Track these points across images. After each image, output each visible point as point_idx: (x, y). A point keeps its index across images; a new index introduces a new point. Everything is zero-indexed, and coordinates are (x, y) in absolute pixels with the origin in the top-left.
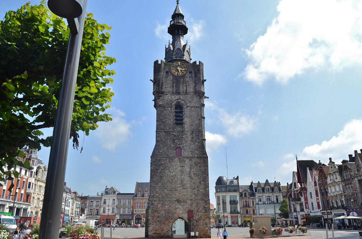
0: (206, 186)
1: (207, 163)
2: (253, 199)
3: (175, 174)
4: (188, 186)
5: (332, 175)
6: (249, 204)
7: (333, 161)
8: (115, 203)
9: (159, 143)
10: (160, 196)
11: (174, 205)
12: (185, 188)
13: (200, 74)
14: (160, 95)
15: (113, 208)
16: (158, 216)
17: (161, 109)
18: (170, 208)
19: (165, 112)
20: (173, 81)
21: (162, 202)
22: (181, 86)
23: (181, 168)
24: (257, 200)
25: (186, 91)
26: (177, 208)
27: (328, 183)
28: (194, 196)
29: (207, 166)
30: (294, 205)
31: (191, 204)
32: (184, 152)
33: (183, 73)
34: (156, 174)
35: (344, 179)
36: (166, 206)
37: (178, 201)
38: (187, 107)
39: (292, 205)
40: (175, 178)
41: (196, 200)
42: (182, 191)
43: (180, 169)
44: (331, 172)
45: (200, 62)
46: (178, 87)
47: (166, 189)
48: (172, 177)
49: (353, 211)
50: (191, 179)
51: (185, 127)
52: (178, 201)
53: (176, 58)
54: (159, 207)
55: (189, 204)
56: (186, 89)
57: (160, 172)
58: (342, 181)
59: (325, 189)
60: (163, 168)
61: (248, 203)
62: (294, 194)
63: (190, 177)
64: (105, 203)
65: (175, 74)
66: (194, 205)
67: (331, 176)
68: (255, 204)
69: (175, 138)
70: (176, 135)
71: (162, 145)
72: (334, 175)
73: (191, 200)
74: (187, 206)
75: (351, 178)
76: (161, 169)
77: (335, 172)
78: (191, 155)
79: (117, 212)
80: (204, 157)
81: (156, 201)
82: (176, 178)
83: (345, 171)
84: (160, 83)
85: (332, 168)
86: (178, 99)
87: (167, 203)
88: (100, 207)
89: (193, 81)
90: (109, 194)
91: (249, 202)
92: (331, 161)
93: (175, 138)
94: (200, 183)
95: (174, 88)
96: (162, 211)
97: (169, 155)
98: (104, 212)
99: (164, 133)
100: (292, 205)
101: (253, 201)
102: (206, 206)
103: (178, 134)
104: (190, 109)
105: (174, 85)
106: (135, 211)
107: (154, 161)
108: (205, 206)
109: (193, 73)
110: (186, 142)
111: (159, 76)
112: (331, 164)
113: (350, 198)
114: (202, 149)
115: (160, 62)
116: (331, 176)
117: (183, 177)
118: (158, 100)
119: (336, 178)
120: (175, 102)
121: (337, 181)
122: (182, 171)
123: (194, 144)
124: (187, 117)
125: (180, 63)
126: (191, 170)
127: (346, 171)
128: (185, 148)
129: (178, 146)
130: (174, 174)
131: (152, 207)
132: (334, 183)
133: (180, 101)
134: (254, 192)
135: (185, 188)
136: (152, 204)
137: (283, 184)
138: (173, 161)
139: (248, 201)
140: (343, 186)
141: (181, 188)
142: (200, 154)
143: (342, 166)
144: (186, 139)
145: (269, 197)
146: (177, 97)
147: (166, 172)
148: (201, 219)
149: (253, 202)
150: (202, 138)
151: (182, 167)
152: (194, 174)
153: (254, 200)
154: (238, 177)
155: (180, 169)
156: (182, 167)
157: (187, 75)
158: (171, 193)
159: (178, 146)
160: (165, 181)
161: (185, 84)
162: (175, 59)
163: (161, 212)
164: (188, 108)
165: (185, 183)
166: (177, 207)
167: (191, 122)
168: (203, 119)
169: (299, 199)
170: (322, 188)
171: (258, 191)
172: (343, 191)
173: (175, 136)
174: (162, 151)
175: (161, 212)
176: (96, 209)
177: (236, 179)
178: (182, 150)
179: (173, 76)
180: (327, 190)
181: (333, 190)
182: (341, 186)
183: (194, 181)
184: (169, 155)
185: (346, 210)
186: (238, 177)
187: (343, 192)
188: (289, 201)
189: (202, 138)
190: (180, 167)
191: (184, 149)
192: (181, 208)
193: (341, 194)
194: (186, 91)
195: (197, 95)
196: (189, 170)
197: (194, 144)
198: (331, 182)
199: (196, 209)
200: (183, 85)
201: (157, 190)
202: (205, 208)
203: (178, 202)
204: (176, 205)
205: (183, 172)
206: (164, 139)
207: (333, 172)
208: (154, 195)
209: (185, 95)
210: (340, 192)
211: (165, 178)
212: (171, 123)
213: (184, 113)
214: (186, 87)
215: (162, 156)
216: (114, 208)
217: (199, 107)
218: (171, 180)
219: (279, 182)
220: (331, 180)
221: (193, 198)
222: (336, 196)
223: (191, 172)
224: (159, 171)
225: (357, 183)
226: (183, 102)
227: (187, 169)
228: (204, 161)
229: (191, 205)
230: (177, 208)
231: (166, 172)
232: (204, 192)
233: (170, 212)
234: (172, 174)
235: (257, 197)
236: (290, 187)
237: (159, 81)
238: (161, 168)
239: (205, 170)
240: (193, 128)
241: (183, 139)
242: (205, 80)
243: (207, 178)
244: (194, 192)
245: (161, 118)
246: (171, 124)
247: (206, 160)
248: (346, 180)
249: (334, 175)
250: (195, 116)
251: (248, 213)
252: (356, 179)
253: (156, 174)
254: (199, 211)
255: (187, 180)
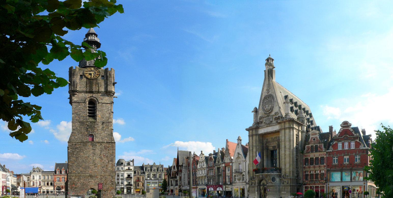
0: (113, 165)
1: (114, 147)
2: (143, 176)
3: (88, 155)
4: (99, 164)
5: (201, 163)
6: (140, 179)
7: (203, 153)
8: (40, 179)
9: (74, 131)
10: (76, 173)
11: (88, 179)
12: (96, 167)
13: (112, 78)
14: (75, 93)
15: (39, 182)
16: (75, 187)
17: (75, 104)
18: (84, 181)
19: (80, 107)
20: (87, 83)
21: (78, 177)
22: (94, 86)
23: (93, 151)
24: (146, 176)
25: (98, 90)
26: (90, 182)
27: (198, 168)
28: (103, 173)
29: (115, 149)
30: (171, 181)
31: (101, 179)
32: (95, 139)
33: (96, 76)
34: (73, 155)
35: (209, 166)
36: (81, 180)
37: (91, 176)
38: (99, 103)
39: (170, 181)
40: (88, 159)
41: (105, 175)
42: (94, 168)
43: (92, 151)
44: (201, 161)
45: (111, 69)
46: (91, 87)
47: (81, 167)
48: (86, 158)
49: (211, 187)
50: (101, 160)
51: (97, 119)
52: (91, 176)
53: (89, 65)
54: (76, 180)
55: (100, 178)
56: (99, 89)
57: (76, 154)
58: (207, 167)
59: (195, 172)
60: (78, 151)
61: (140, 179)
62: (173, 174)
63: (101, 158)
64: (34, 179)
65: (88, 77)
66: (103, 179)
67: (201, 163)
68: (144, 180)
69: (88, 127)
70: (89, 125)
71: (77, 133)
72: (203, 163)
73: (101, 175)
74: (98, 180)
75: (213, 165)
76: (77, 152)
77: (203, 161)
78: (101, 141)
79: (43, 185)
80: (112, 143)
81: (73, 176)
82: (89, 159)
83: (210, 161)
84: (75, 84)
85: (202, 158)
86: (91, 97)
87: (82, 178)
88: (31, 181)
89: (105, 83)
90: (36, 172)
91: (140, 178)
92: (202, 153)
93: (88, 127)
94: (109, 162)
95: (88, 88)
96: (78, 183)
97: (83, 141)
98: (34, 185)
99: (78, 123)
100: (170, 181)
101: (143, 177)
102: (113, 180)
103: (91, 124)
104: (101, 105)
105: (88, 86)
106: (55, 184)
107: (71, 145)
108: (112, 180)
109: (105, 77)
110: (98, 130)
111: (74, 79)
112: (201, 155)
113: (210, 179)
114: (111, 137)
115: (74, 68)
116: (201, 163)
117: (94, 158)
118: (73, 98)
119: (204, 165)
120: (88, 99)
121: (204, 167)
122: (94, 154)
123: (104, 132)
124: (99, 111)
125: (93, 68)
126: (101, 152)
127: (211, 161)
128: (96, 135)
129: (91, 133)
130: (87, 155)
131: (70, 180)
132: (202, 168)
133: (93, 98)
134: (144, 171)
135: (96, 167)
136: (70, 179)
137: (166, 166)
138: (87, 145)
139: (140, 177)
140: (207, 171)
141: (93, 167)
142: (109, 140)
143: (209, 158)
144: (97, 128)
145: (160, 175)
146: (90, 95)
147: (81, 154)
148: (108, 189)
149: (143, 178)
150: (111, 128)
151: (94, 150)
152: (104, 156)
153: (144, 177)
154: (133, 160)
155: (92, 151)
156: (94, 150)
157: (99, 78)
158: (85, 170)
159: (91, 133)
160: (81, 161)
161: (97, 85)
162: (88, 65)
163: (78, 184)
164: (100, 104)
165: (96, 162)
166: (90, 180)
167: (102, 115)
168: (112, 113)
169: (176, 177)
170: (193, 171)
171: (147, 170)
172: (207, 174)
173: (88, 126)
174: (77, 137)
175: (78, 184)
176: (28, 183)
177: (132, 161)
178: (94, 137)
179: (87, 78)
180: (196, 172)
181: (200, 173)
182: (206, 171)
183: (104, 161)
184: (83, 141)
185: (207, 186)
186: (133, 160)
187: (206, 175)
188: (169, 178)
189: (111, 128)
190: (93, 150)
191: (96, 136)
192: (93, 181)
193: (205, 176)
194: (98, 90)
195: (108, 94)
196: (99, 152)
197: (104, 132)
198: (200, 168)
199: (105, 182)
200: (96, 85)
201: (74, 168)
202: (112, 181)
203: (90, 177)
204: (89, 180)
205: (95, 154)
206: (79, 128)
207: (202, 161)
208: (72, 172)
209: (97, 93)
210: (205, 175)
211: (80, 159)
212: (85, 115)
213: (96, 108)
214: (99, 87)
215: (78, 141)
216: (40, 182)
217: (109, 104)
218: (85, 160)
219: (163, 165)
220: (200, 166)
221: (102, 174)
222: (202, 177)
223: (102, 154)
224: (75, 153)
225: (216, 169)
226: (95, 99)
227: (98, 151)
228: (112, 146)
229: (101, 179)
230: (90, 182)
231: (81, 154)
232: (111, 170)
233: (85, 185)
234: (85, 155)
235: (146, 174)
236: (170, 168)
237: (74, 82)
238: (77, 151)
239: (113, 152)
240: (103, 120)
241: (95, 128)
242: (116, 83)
243: (114, 159)
244: (104, 170)
245: (76, 111)
246: (84, 116)
247: (114, 145)
248: (210, 167)
249: (203, 163)
250: (106, 110)
251: (139, 186)
252: (216, 167)
253: (73, 155)
254: (107, 184)
255: (98, 160)
